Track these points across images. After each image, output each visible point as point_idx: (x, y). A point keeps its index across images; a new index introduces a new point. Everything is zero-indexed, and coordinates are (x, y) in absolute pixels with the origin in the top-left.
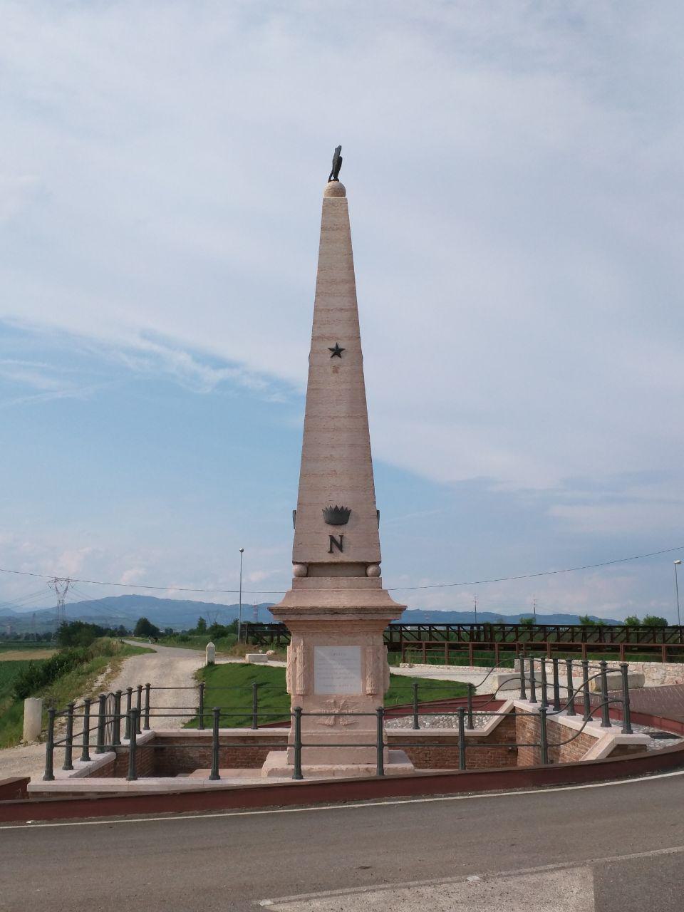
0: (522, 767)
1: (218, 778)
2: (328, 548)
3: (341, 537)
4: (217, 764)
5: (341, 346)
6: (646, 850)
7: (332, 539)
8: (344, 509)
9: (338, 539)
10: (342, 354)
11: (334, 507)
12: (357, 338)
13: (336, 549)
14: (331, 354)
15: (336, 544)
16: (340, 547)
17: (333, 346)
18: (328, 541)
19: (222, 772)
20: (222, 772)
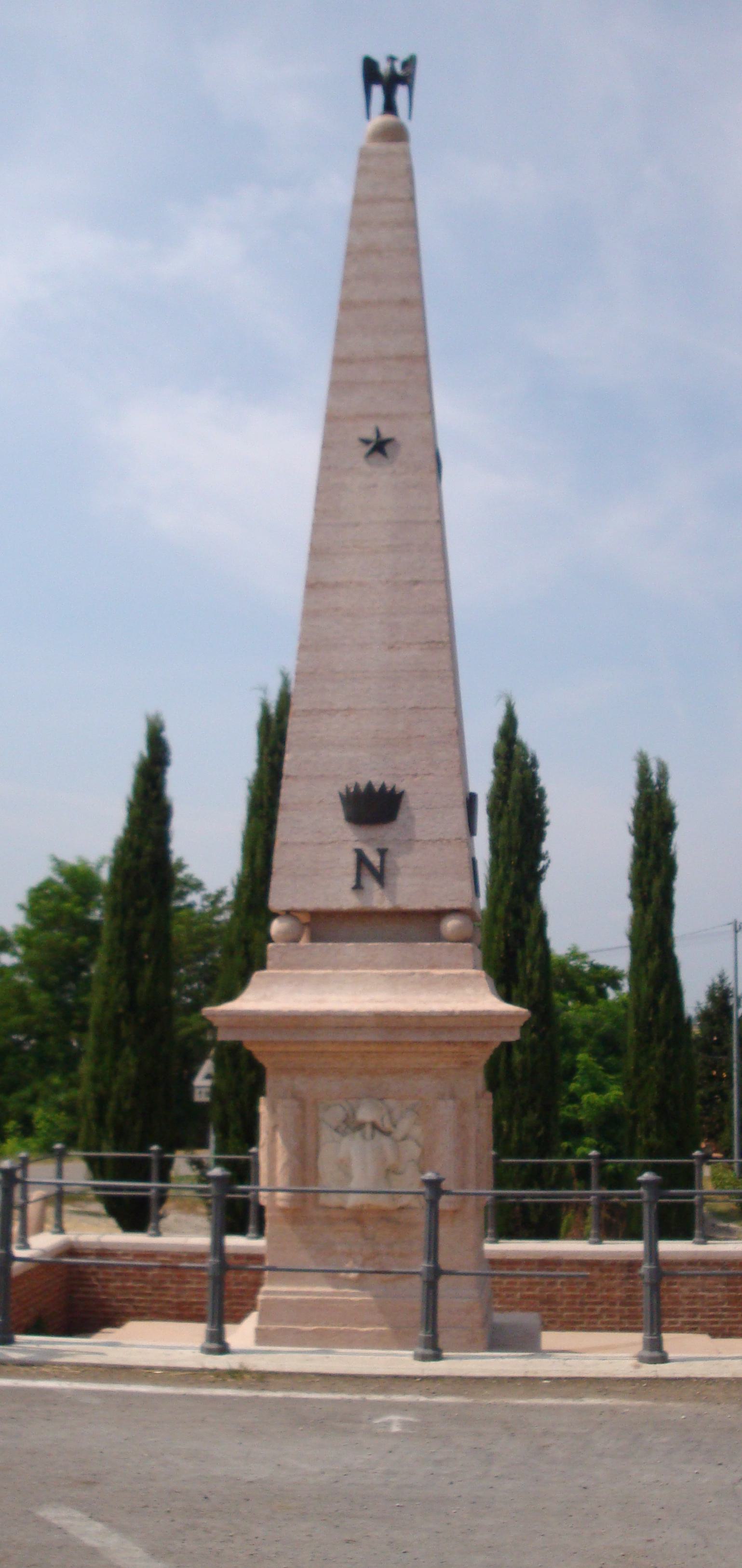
0: (701, 1174)
1: (664, 1359)
2: (351, 881)
3: (382, 852)
4: (659, 1324)
5: (385, 434)
6: (350, 1401)
7: (361, 860)
8: (377, 788)
9: (374, 859)
10: (388, 448)
11: (363, 787)
12: (326, 467)
13: (370, 883)
14: (367, 449)
15: (370, 870)
16: (380, 877)
17: (370, 435)
18: (351, 859)
19: (671, 1341)
20: (671, 1341)
